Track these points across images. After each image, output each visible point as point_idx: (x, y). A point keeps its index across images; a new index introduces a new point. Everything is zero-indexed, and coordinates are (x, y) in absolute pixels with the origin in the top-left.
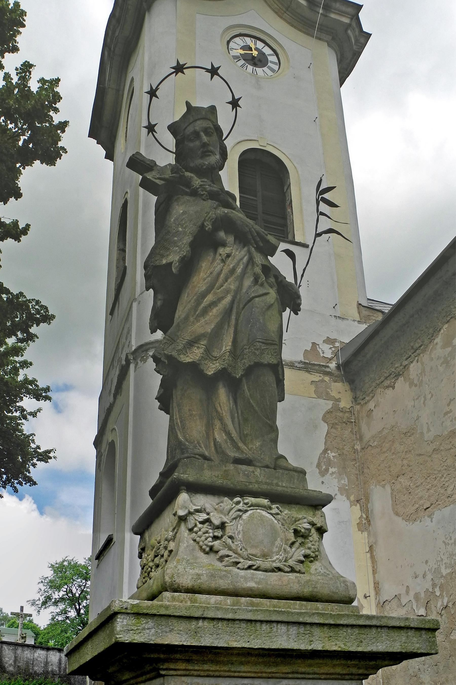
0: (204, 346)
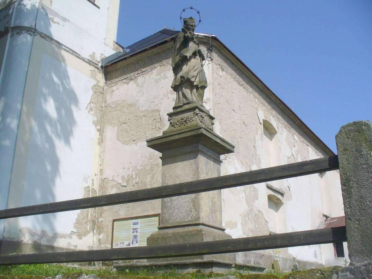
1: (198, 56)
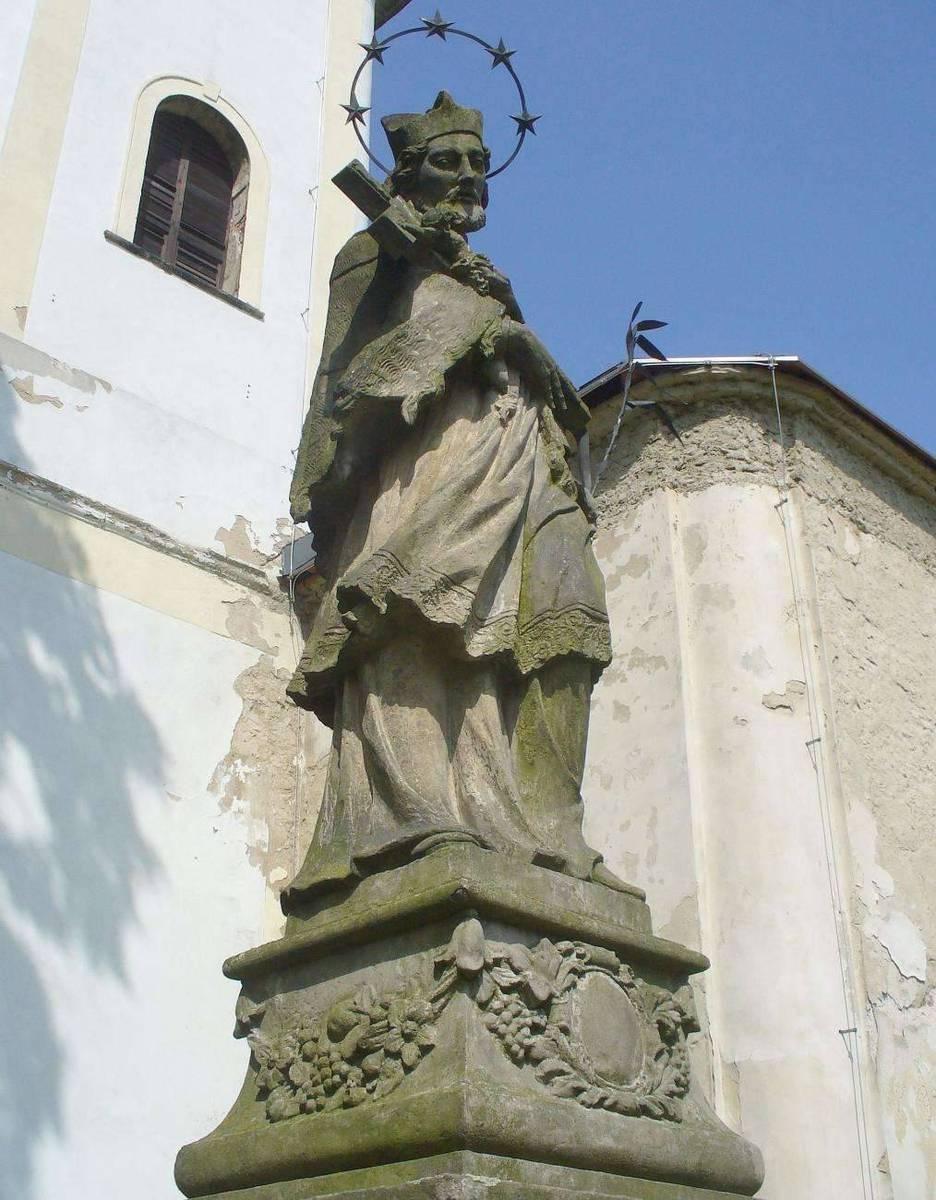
0: (472, 595)
1: (513, 389)
